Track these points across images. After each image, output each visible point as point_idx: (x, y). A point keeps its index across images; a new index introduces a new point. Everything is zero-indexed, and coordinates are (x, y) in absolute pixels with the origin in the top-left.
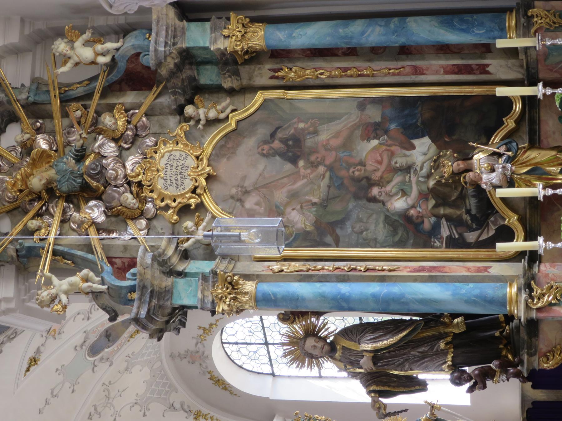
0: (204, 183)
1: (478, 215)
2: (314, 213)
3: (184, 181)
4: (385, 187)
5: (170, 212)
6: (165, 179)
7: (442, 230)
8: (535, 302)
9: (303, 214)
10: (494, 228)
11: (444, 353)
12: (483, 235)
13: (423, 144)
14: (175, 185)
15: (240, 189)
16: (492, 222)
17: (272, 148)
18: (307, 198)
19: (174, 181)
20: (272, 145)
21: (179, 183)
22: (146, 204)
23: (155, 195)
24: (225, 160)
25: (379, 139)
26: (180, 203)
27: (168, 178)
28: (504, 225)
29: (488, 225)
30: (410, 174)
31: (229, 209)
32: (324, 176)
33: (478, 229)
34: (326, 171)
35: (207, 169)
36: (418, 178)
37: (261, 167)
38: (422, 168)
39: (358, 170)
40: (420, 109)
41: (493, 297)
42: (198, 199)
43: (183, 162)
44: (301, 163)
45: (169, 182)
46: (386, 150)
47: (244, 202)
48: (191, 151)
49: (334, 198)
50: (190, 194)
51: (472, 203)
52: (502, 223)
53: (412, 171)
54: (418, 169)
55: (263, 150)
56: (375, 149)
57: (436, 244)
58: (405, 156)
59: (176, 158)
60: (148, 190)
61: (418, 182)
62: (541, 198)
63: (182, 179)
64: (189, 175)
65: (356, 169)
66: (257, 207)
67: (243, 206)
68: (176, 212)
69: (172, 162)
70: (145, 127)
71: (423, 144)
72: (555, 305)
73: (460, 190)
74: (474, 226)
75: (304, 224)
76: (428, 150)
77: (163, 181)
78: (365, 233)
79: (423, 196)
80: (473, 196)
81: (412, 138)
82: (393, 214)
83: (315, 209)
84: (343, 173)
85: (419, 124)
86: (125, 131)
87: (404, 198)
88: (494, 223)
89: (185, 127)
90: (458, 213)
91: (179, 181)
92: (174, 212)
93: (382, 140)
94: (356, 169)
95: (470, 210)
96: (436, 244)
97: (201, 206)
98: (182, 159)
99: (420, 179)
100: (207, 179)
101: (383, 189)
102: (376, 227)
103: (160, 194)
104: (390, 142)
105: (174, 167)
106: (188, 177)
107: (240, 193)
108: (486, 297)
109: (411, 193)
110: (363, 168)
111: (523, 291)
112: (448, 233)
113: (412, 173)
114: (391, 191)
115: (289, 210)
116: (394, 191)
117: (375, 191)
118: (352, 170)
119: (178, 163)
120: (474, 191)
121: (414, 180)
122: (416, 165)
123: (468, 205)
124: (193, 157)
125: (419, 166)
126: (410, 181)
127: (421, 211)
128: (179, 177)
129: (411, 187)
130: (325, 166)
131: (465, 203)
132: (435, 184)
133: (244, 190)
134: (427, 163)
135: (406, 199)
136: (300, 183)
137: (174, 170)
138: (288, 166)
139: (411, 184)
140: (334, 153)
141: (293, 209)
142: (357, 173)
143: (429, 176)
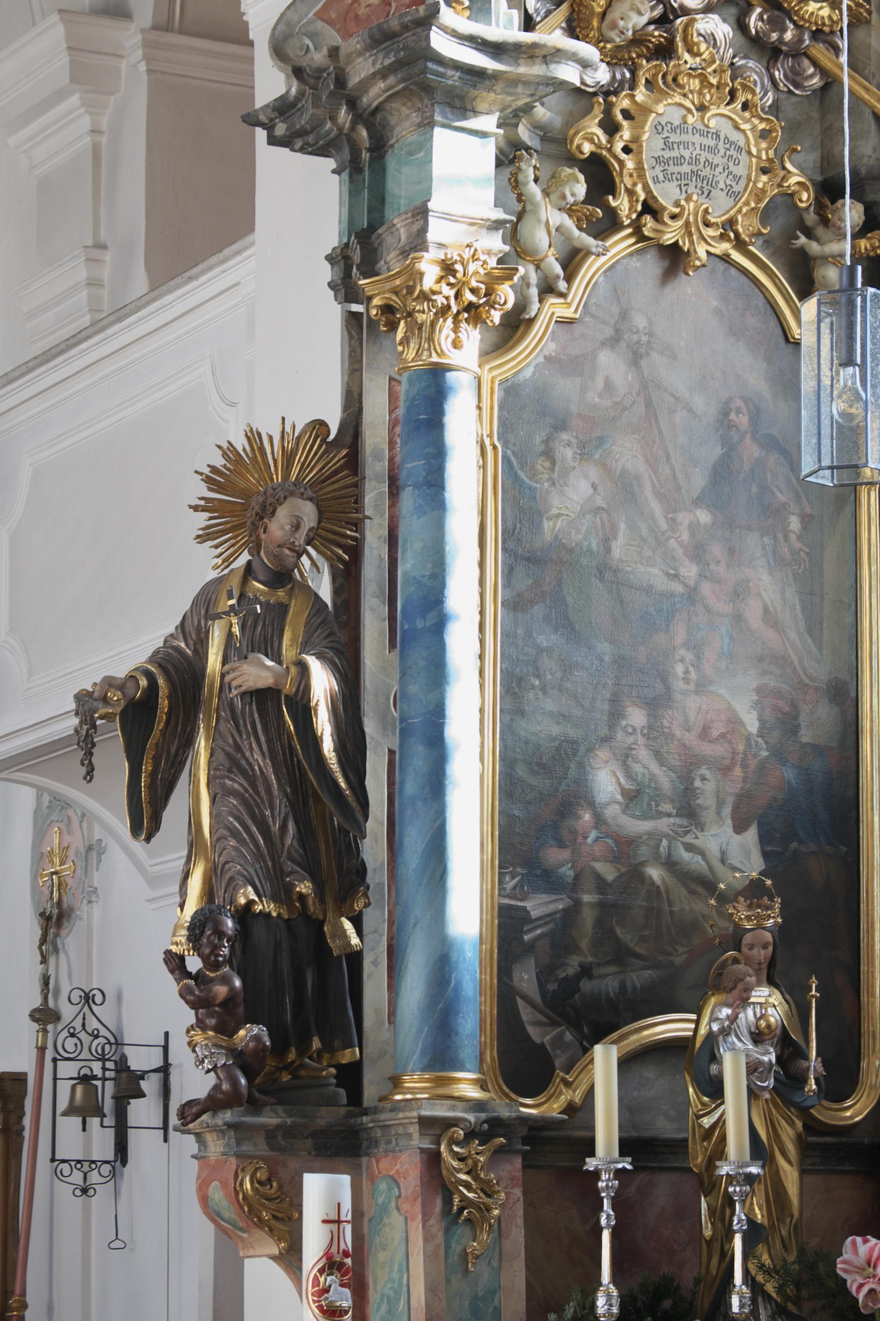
0: (668, 238)
1: (576, 997)
2: (586, 544)
3: (675, 183)
4: (646, 746)
5: (599, 132)
6: (682, 127)
7: (544, 897)
8: (456, 1149)
9: (582, 514)
10: (547, 1039)
11: (281, 892)
12: (530, 1009)
13: (748, 856)
14: (667, 154)
15: (645, 339)
16: (561, 1035)
17: (742, 439)
18: (623, 526)
19: (675, 154)
20: (748, 440)
21: (672, 169)
22: (608, 63)
23: (641, 94)
24: (715, 303)
25: (760, 734)
26: (621, 163)
27: (685, 138)
28: (553, 1069)
29: (555, 1024)
30: (677, 815)
31: (597, 305)
32: (676, 577)
33: (543, 998)
34: (685, 585)
35: (701, 251)
36: (667, 836)
37: (699, 403)
38: (689, 848)
39: (687, 672)
40: (829, 849)
41: (457, 1034)
42: (628, 217)
43: (722, 185)
44: (704, 517)
45: (674, 138)
46: (734, 753)
47: (612, 347)
48: (744, 210)
49: (622, 603)
50: (642, 198)
51: (607, 983)
52: (557, 1063)
53: (684, 822)
54: (688, 839)
55: (738, 411)
56: (735, 722)
57: (507, 878)
58: (720, 803)
59: (731, 164)
60: (655, 76)
61: (655, 837)
62: (591, 1164)
63: (681, 176)
64: (688, 199)
65: (691, 669)
66: (600, 384)
67: (603, 344)
68: (598, 151)
69: (722, 152)
70: (796, 78)
71: (748, 856)
72: (448, 1202)
73: (639, 950)
74: (552, 987)
75: (560, 515)
76: (735, 869)
77: (677, 122)
78: (537, 683)
79: (623, 848)
80: (623, 987)
81: (760, 826)
82: (581, 765)
83: (594, 546)
84: (680, 633)
85: (794, 845)
86: (795, 23)
87: (619, 797)
88: (558, 1041)
89: (805, 196)
90: (584, 944)
91: (676, 169)
92: (599, 146)
93: (756, 742)
94: (691, 669)
95: (591, 977)
96: (507, 878)
97: (609, 225)
98: (728, 182)
99: (665, 843)
100: (675, 247)
101: (641, 741)
102: (551, 714)
103: (645, 110)
104: (753, 763)
105: (710, 157)
106: (684, 195)
107: (635, 338)
108: (457, 1013)
109: (634, 817)
110: (692, 687)
111: (483, 1116)
112: (534, 914)
113: (678, 821)
114: (637, 761)
115: (594, 473)
116: (637, 768)
117: (637, 717)
118: (689, 656)
119: (720, 169)
120: (635, 988)
121: (664, 825)
122: (699, 834)
123: (603, 971)
124: (732, 212)
125: (693, 841)
126: (661, 815)
127: (589, 840)
128: (686, 168)
129: (645, 817)
130: (697, 584)
131: (608, 963)
132: (652, 883)
133: (642, 351)
134: (703, 863)
135: (618, 803)
136: (655, 507)
137: (704, 156)
138: (699, 480)
139: (652, 818)
140: (728, 608)
141: (594, 486)
142: (679, 669)
143: (671, 864)
